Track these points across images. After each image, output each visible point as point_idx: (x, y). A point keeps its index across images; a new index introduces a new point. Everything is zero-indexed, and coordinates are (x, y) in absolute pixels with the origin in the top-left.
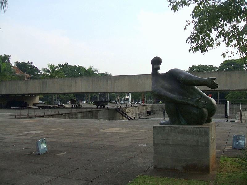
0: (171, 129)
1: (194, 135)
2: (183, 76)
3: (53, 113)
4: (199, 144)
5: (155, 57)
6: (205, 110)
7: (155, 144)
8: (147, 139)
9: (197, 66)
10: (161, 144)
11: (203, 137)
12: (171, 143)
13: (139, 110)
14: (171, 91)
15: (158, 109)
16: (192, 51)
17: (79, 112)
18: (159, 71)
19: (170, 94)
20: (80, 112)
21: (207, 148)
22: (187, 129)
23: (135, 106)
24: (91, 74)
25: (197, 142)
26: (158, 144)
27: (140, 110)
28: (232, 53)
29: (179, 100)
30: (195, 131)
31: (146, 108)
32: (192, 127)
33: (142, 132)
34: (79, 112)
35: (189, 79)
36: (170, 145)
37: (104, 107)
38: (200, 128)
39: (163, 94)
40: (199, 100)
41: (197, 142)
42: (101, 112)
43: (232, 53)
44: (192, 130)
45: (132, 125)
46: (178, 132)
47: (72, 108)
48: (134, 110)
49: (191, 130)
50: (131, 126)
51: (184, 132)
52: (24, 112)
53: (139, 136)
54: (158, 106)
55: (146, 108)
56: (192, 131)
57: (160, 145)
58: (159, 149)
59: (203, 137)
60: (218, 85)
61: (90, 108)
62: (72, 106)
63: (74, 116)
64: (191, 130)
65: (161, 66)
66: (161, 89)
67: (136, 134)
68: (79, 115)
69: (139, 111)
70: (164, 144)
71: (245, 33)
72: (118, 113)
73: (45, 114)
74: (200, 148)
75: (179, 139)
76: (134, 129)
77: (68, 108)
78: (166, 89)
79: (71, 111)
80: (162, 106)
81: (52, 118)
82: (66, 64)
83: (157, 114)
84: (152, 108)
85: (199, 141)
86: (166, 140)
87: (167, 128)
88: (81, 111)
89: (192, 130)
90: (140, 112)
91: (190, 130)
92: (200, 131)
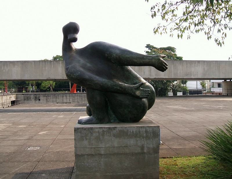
0: (103, 131)
1: (138, 139)
2: (118, 52)
4: (145, 151)
6: (145, 100)
7: (77, 156)
10: (87, 155)
11: (151, 140)
12: (103, 152)
13: (2, 100)
15: (23, 98)
19: (97, 77)
25: (142, 148)
26: (83, 155)
27: (3, 99)
30: (139, 132)
31: (10, 98)
33: (21, 128)
35: (128, 56)
36: (101, 155)
38: (147, 128)
39: (87, 77)
41: (142, 148)
44: (134, 131)
45: (5, 119)
46: (114, 136)
49: (133, 132)
50: (4, 121)
51: (123, 134)
53: (21, 134)
54: (23, 95)
55: (10, 98)
56: (134, 133)
57: (86, 156)
59: (151, 140)
60: (167, 65)
61: (190, 98)
64: (133, 132)
65: (78, 36)
66: (82, 69)
67: (16, 132)
69: (2, 101)
70: (92, 155)
74: (146, 156)
76: (11, 125)
78: (89, 70)
80: (27, 95)
83: (22, 103)
84: (17, 98)
85: (145, 146)
87: (97, 130)
89: (134, 131)
90: (3, 102)
92: (146, 132)
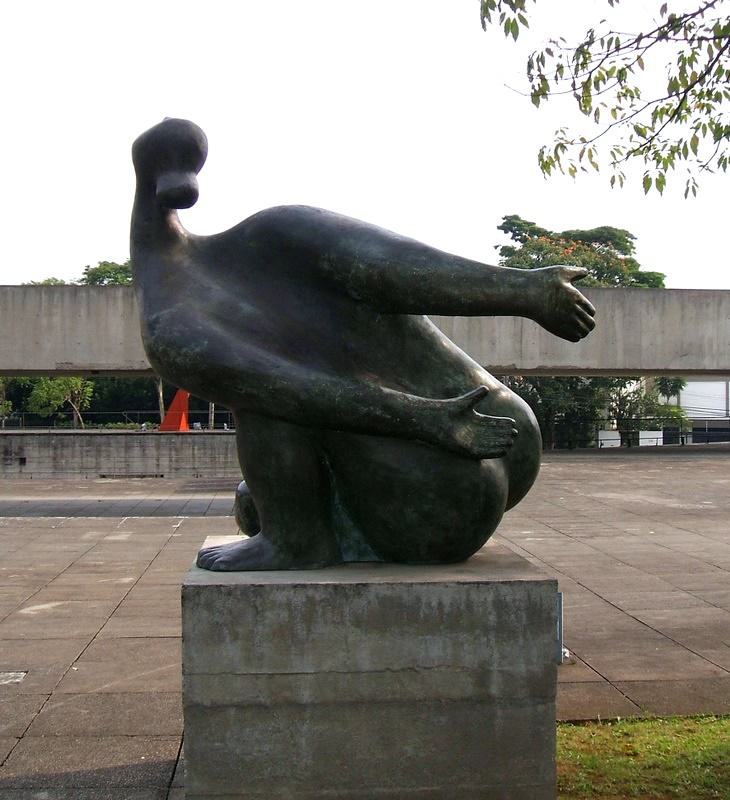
0: (310, 601)
1: (463, 636)
4: (494, 690)
5: (131, 147)
7: (193, 710)
8: (62, 580)
9: (121, 268)
10: (240, 707)
11: (521, 641)
12: (306, 696)
14: (293, 346)
18: (180, 212)
19: (286, 365)
21: (541, 708)
22: (418, 599)
25: (482, 676)
28: (586, 154)
29: (709, 462)
30: (469, 605)
32: (445, 585)
35: (417, 270)
36: (300, 707)
38: (505, 589)
40: (470, 407)
41: (482, 676)
43: (586, 154)
44: (447, 601)
46: (358, 622)
49: (440, 604)
56: (447, 609)
57: (232, 712)
58: (223, 740)
64: (440, 604)
65: (203, 180)
66: (217, 329)
74: (499, 712)
75: (366, 665)
78: (250, 330)
85: (495, 667)
86: (271, 676)
87: (281, 597)
89: (447, 601)
91: (434, 604)
92: (500, 605)
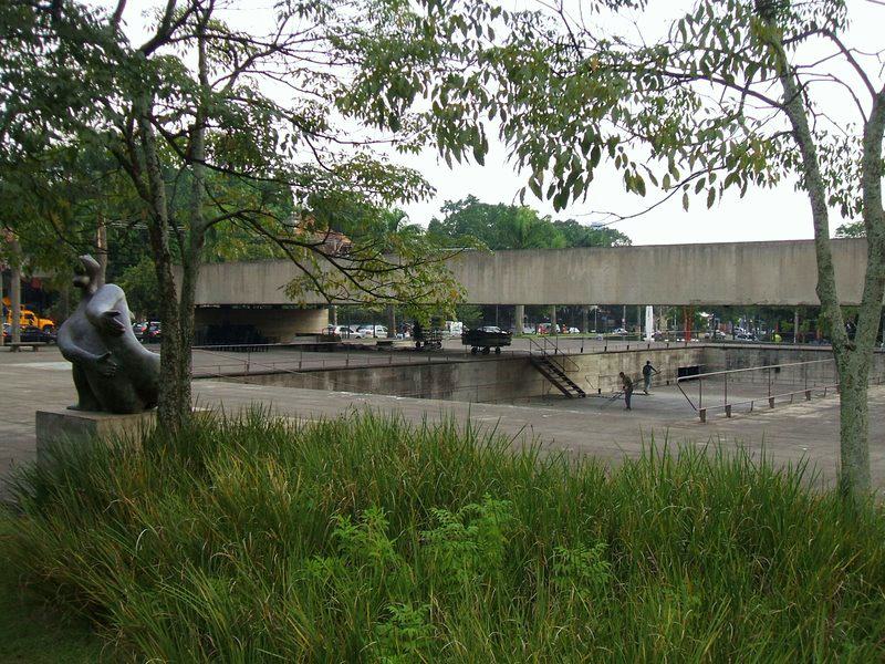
3: (280, 367)
16: (395, 146)
17: (376, 367)
20: (380, 367)
23: (625, 348)
24: (525, 234)
31: (675, 357)
34: (376, 367)
37: (498, 351)
42: (464, 367)
47: (417, 350)
48: (613, 365)
52: (260, 361)
54: (723, 352)
62: (418, 344)
63: (354, 378)
68: (375, 376)
71: (370, 80)
72: (540, 376)
73: (251, 370)
77: (406, 350)
79: (390, 359)
80: (737, 351)
81: (264, 383)
82: (472, 199)
88: (386, 362)
